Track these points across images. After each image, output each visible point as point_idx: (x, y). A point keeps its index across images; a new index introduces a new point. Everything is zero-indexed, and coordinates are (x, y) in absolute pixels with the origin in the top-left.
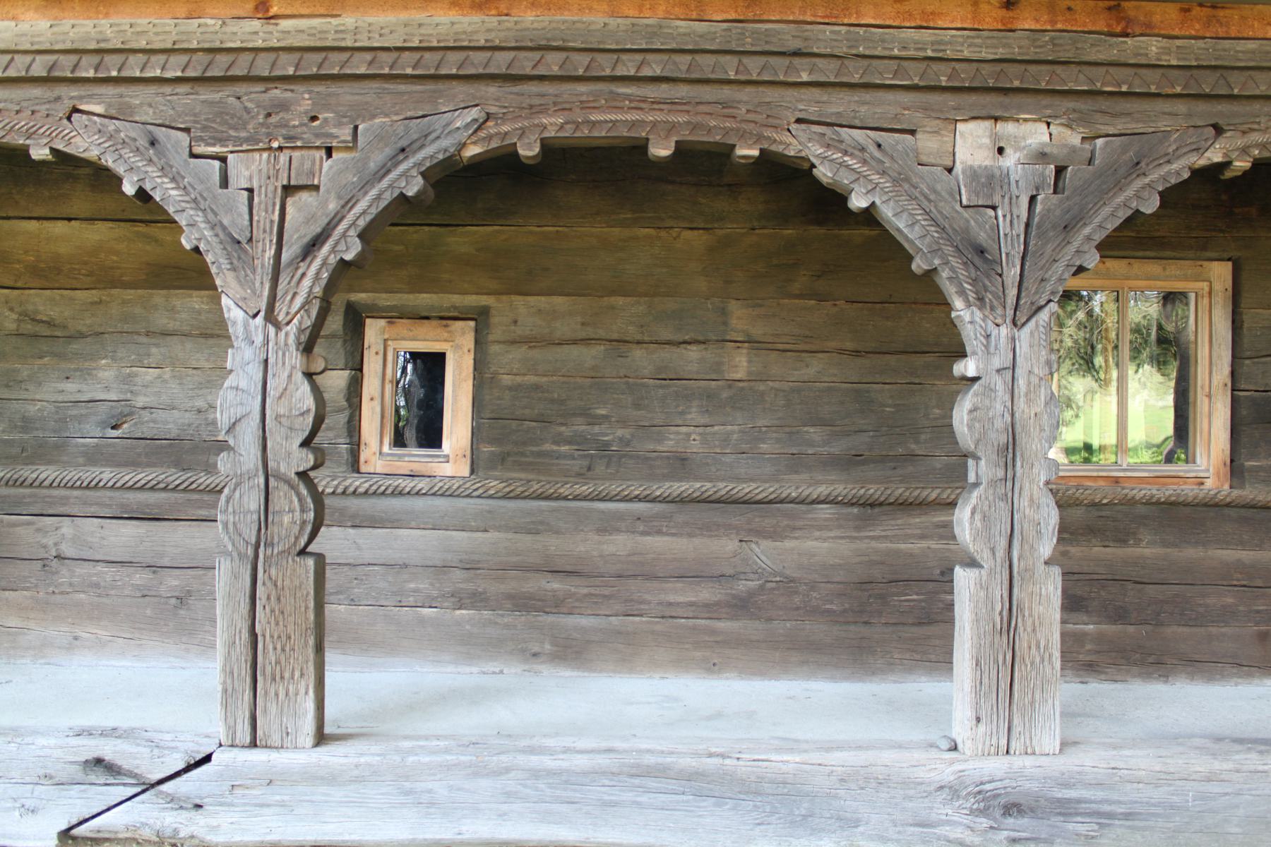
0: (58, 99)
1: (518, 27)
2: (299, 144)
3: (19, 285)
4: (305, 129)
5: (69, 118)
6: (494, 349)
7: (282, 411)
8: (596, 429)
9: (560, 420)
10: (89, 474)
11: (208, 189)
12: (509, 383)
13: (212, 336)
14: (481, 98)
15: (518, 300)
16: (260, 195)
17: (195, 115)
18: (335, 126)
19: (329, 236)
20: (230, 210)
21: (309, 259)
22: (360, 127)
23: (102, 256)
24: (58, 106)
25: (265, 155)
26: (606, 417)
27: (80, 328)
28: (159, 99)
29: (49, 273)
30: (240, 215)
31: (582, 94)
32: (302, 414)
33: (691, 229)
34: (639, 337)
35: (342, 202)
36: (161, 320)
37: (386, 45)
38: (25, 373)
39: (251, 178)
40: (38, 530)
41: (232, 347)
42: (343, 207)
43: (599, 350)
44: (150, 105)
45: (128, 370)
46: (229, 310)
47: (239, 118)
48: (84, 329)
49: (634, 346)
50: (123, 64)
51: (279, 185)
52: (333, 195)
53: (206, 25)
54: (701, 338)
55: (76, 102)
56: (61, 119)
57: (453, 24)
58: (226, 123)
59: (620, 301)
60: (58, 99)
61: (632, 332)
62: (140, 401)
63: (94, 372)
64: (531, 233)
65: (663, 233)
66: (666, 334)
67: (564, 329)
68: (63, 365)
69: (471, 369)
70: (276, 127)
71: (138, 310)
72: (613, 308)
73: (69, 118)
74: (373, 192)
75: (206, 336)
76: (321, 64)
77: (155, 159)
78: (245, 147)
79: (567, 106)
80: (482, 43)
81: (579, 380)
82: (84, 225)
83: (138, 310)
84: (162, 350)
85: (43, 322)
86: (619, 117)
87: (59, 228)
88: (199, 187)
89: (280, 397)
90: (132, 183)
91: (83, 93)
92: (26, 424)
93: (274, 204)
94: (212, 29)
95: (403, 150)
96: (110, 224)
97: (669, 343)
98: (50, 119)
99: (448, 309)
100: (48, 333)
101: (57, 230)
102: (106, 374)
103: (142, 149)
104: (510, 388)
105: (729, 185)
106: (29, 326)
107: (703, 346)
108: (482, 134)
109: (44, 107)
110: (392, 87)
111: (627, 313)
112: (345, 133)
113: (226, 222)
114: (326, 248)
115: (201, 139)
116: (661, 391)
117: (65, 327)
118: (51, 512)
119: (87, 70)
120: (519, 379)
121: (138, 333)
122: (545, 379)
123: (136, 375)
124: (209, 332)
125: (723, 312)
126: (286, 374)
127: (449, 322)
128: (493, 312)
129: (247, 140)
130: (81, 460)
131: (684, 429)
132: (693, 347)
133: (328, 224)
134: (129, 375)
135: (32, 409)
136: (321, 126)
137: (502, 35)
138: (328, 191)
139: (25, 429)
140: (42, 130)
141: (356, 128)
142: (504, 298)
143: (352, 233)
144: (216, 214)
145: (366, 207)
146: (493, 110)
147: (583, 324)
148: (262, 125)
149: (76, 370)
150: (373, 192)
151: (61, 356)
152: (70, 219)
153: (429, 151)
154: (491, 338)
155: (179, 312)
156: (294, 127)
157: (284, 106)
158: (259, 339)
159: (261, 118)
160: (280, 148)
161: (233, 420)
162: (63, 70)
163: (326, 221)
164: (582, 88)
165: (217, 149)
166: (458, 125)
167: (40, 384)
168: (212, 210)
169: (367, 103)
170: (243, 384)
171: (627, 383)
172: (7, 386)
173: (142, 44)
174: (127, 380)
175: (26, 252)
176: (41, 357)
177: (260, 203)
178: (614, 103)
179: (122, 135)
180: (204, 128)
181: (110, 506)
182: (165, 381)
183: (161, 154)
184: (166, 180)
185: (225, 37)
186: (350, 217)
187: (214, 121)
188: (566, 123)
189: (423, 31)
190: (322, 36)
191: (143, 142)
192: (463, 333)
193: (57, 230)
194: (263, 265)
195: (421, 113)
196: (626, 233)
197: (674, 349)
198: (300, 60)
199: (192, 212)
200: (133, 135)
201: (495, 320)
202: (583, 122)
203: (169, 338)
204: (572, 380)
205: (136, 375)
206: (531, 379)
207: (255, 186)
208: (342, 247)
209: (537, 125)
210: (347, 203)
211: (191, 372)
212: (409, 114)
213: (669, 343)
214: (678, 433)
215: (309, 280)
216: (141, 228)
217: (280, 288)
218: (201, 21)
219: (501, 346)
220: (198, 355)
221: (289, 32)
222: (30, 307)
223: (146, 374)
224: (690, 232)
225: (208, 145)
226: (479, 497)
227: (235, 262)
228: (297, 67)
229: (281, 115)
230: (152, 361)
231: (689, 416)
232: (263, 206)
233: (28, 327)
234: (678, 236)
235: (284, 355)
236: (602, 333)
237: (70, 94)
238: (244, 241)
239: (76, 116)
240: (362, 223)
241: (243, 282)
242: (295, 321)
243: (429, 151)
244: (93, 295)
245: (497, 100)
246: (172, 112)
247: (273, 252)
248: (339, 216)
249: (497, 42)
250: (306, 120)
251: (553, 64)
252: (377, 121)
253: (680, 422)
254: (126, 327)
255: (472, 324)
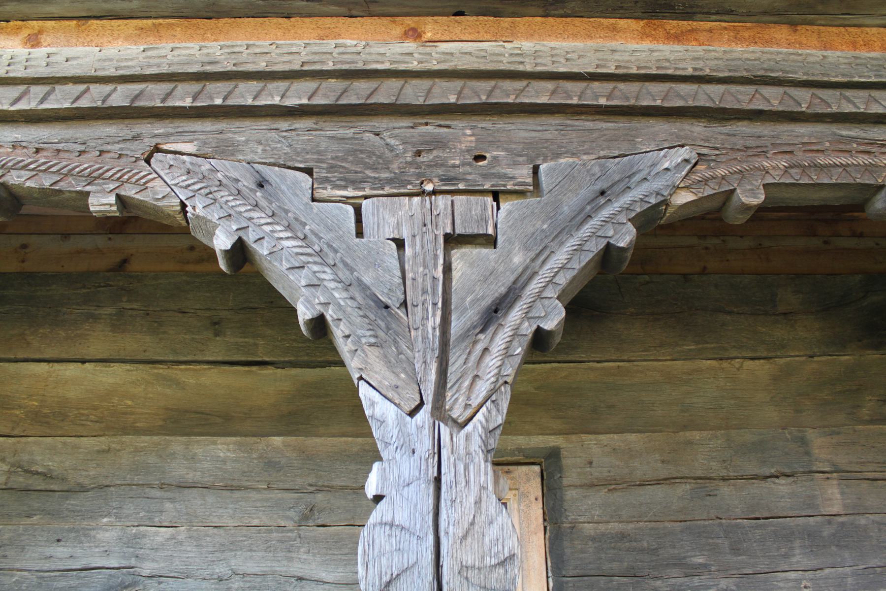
0: (135, 138)
1: (728, 56)
2: (461, 186)
3: (15, 433)
4: (468, 169)
5: (148, 161)
6: (570, 494)
7: (469, 560)
8: (696, 581)
9: (653, 573)
11: (340, 238)
12: (592, 533)
13: (238, 488)
14: (686, 138)
15: (589, 440)
16: (413, 245)
17: (319, 153)
18: (509, 166)
19: (518, 297)
20: (375, 265)
21: (491, 330)
22: (543, 167)
23: (115, 400)
24: (135, 145)
25: (416, 200)
26: (705, 566)
27: (81, 480)
28: (273, 134)
29: (52, 419)
30: (388, 270)
31: (803, 136)
32: (502, 564)
33: (752, 359)
34: (723, 473)
35: (532, 254)
36: (179, 470)
37: (576, 70)
38: (7, 536)
39: (398, 226)
41: (380, 459)
42: (533, 260)
43: (682, 489)
44: (260, 143)
46: (373, 404)
47: (380, 157)
48: (87, 482)
49: (721, 483)
50: (230, 93)
51: (440, 233)
52: (517, 246)
53: (345, 46)
54: (787, 471)
55: (158, 140)
56: (137, 159)
57: (652, 51)
58: (360, 162)
59: (696, 435)
60: (135, 138)
61: (716, 468)
62: (147, 568)
63: (92, 533)
64: (591, 369)
65: (725, 364)
66: (752, 468)
67: (642, 469)
69: (541, 520)
70: (429, 166)
71: (152, 459)
72: (690, 443)
73: (148, 161)
74: (572, 243)
75: (231, 488)
76: (491, 91)
77: (263, 203)
78: (388, 190)
79: (789, 149)
80: (690, 72)
81: (667, 524)
82: (99, 367)
83: (152, 459)
84: (177, 504)
85: (38, 473)
86: (850, 161)
87: (71, 370)
88: (327, 236)
89: (465, 537)
90: (229, 233)
91: (171, 130)
93: (436, 257)
94: (354, 50)
95: (603, 193)
96: (128, 367)
97: (755, 477)
98: (123, 160)
99: (512, 453)
100: (42, 487)
101: (67, 373)
102: (107, 535)
103: (245, 191)
104: (593, 539)
105: (785, 314)
106: (21, 479)
107: (791, 479)
108: (696, 177)
109: (117, 146)
110: (577, 123)
111: (706, 452)
112: (524, 174)
113: (367, 279)
114: (515, 315)
115: (327, 180)
116: (758, 532)
117: (64, 480)
119: (183, 99)
120: (602, 527)
121: (151, 486)
122: (631, 526)
123: (144, 536)
124: (235, 483)
125: (803, 441)
126: (472, 500)
127: (511, 468)
128: (564, 453)
129: (390, 182)
131: (792, 575)
132: (782, 481)
133: (514, 282)
134: (135, 536)
136: (491, 166)
137: (712, 63)
138: (510, 241)
140: (110, 173)
141: (536, 170)
142: (574, 437)
143: (551, 293)
144: (351, 270)
145: (567, 262)
146: (704, 151)
147: (663, 462)
148: (410, 164)
149: (70, 530)
150: (572, 243)
151: (54, 514)
152: (83, 362)
153: (636, 193)
154: (565, 481)
155: (200, 461)
156: (454, 166)
157: (440, 144)
158: (425, 445)
159: (409, 156)
160: (434, 192)
161: (386, 579)
162: (152, 99)
163: (512, 278)
164: (803, 130)
165: (350, 192)
166: (666, 165)
167: (23, 549)
168: (346, 264)
169: (547, 141)
170: (401, 518)
171: (721, 525)
173: (261, 66)
174: (133, 542)
175: (30, 396)
177: (415, 256)
178: (842, 146)
179: (219, 176)
180: (332, 168)
182: (179, 543)
183: (269, 198)
184: (278, 228)
185: (369, 58)
186: (545, 272)
187: (343, 160)
188: (791, 167)
189: (617, 57)
190: (495, 58)
191: (247, 183)
192: (528, 480)
193: (67, 373)
194: (425, 338)
195: (617, 153)
196: (689, 365)
197: (763, 484)
198: (462, 88)
199: (316, 268)
200: (234, 174)
201: (566, 462)
202: (810, 166)
203: (186, 491)
204: (660, 525)
205: (144, 536)
206: (615, 527)
207: (405, 234)
208: (538, 311)
209: (758, 169)
210: (538, 255)
211: (211, 531)
212: (602, 153)
213: (755, 477)
214: (787, 580)
215: (496, 358)
216: (161, 370)
217: (451, 370)
218: (337, 41)
219: (579, 490)
220: (221, 511)
221: (452, 54)
222: (26, 457)
223: (156, 534)
224: (751, 362)
225: (336, 187)
227: (381, 334)
228: (459, 94)
229: (435, 153)
230: (165, 519)
231: (794, 560)
232: (420, 259)
233: (20, 480)
234: (741, 367)
235: (466, 468)
236: (684, 471)
237: (151, 131)
238: (394, 303)
239: (158, 156)
240: (563, 280)
241: (399, 362)
242: (479, 416)
243: (636, 193)
244: (103, 442)
245: (707, 140)
246: (288, 150)
247: (438, 320)
248: (529, 272)
249: (707, 72)
250: (469, 158)
251: (772, 98)
252: (563, 161)
253: (786, 568)
254: (136, 479)
255: (537, 468)
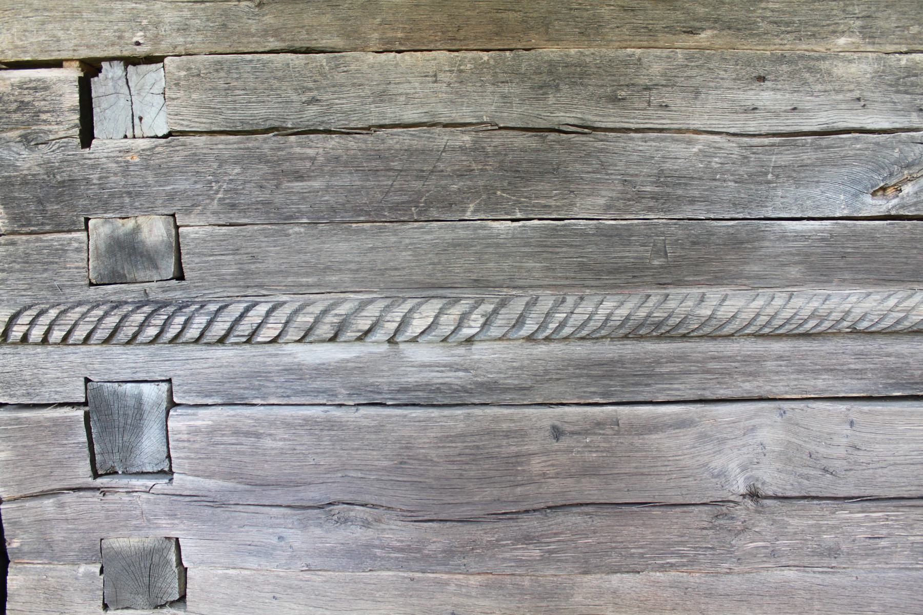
10: (807, 302)
40: (703, 437)
45: (904, 60)
68: (749, 48)
92: (669, 188)
102: (853, 69)
118: (722, 393)
130: (794, 272)
135: (682, 154)
139: (662, 201)
167: (697, 93)
172: (614, 99)
176: (692, 32)
181: (858, 373)
226: (547, 339)
